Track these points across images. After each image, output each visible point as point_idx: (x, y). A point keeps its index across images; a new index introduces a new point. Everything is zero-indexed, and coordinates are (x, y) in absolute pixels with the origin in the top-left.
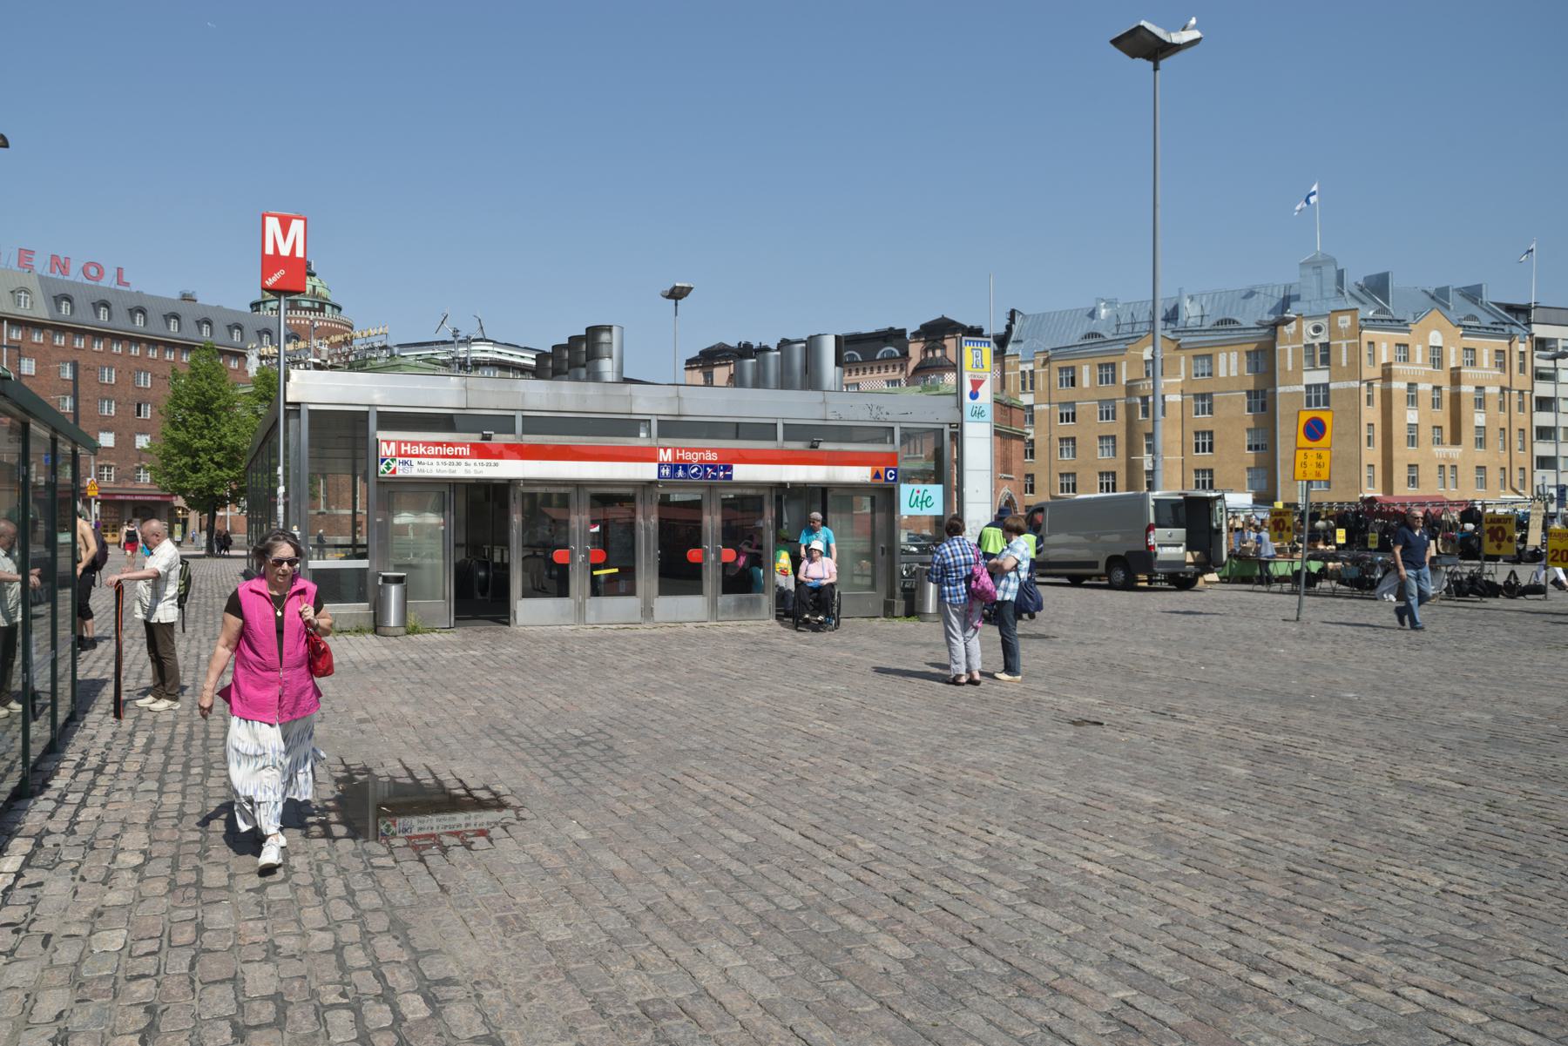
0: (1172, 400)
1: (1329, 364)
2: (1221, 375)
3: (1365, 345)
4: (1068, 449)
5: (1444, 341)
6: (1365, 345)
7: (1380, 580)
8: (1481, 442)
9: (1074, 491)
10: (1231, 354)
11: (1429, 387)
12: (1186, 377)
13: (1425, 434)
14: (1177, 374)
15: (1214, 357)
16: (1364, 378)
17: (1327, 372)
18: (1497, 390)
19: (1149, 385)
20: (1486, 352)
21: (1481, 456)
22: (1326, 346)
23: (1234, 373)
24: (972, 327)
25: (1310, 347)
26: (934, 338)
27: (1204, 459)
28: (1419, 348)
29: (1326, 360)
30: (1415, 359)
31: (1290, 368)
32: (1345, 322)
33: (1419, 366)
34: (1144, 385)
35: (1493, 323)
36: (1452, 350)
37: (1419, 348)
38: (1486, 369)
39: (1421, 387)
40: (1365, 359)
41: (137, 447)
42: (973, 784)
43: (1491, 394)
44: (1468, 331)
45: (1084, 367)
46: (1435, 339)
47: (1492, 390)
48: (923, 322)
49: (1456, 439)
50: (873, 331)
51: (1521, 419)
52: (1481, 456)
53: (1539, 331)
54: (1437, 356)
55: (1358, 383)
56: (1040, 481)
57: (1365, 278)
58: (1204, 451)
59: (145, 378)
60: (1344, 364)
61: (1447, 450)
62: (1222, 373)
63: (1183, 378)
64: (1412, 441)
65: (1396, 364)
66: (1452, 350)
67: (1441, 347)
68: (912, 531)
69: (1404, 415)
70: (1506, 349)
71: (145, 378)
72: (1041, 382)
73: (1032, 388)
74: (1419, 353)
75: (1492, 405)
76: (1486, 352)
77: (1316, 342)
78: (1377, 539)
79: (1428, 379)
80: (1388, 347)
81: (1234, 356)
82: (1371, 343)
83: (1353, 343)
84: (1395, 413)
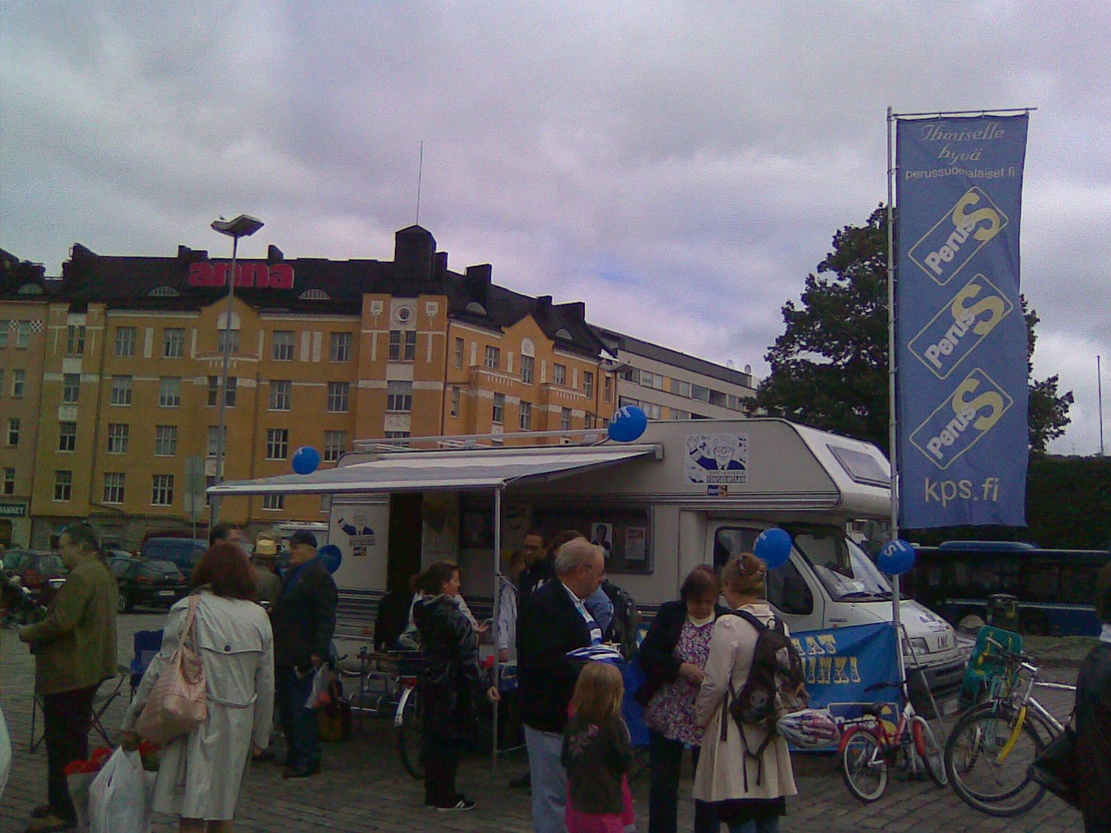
1: (414, 359)
3: (453, 342)
4: (118, 440)
6: (453, 342)
9: (121, 499)
10: (316, 333)
11: (517, 401)
16: (449, 380)
17: (411, 368)
19: (219, 362)
20: (575, 372)
22: (411, 336)
23: (317, 359)
25: (395, 334)
28: (510, 355)
29: (410, 353)
30: (506, 367)
31: (374, 358)
32: (431, 308)
33: (509, 375)
36: (544, 363)
37: (510, 355)
38: (574, 390)
39: (508, 399)
40: (453, 359)
42: (968, 738)
54: (528, 366)
55: (440, 386)
56: (79, 481)
57: (45, 269)
58: (277, 456)
59: (1011, 174)
62: (304, 357)
63: (261, 357)
65: (484, 369)
66: (544, 363)
67: (532, 359)
70: (594, 372)
71: (1011, 174)
72: (92, 345)
76: (575, 372)
77: (403, 329)
78: (373, 630)
80: (478, 349)
81: (318, 337)
82: (460, 340)
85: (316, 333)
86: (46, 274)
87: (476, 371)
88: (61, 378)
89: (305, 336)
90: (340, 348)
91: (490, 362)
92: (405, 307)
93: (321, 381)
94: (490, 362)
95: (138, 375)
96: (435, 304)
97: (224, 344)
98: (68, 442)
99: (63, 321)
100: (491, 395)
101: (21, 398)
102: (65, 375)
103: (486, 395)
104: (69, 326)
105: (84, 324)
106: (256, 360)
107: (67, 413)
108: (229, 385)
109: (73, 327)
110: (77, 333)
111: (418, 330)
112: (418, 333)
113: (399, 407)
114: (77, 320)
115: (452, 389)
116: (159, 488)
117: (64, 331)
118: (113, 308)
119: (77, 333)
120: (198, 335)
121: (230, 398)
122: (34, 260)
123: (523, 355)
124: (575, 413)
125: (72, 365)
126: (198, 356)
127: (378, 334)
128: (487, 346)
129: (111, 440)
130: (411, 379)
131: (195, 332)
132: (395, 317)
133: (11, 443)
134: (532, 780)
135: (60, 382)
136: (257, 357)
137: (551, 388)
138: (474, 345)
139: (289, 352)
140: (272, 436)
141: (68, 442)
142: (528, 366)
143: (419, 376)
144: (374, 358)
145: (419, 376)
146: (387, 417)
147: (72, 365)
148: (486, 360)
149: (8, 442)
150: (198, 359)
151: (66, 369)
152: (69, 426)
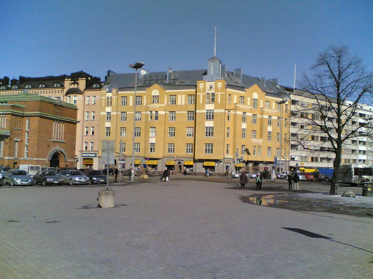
0: (161, 113)
2: (179, 104)
3: (227, 95)
5: (160, 94)
7: (16, 185)
8: (269, 138)
10: (183, 95)
11: (251, 114)
12: (167, 104)
13: (248, 133)
14: (163, 103)
15: (177, 96)
18: (276, 118)
21: (270, 143)
23: (183, 104)
24: (96, 77)
26: (75, 79)
27: (172, 139)
28: (249, 99)
30: (247, 103)
31: (201, 103)
32: (201, 85)
34: (151, 106)
35: (278, 93)
36: (262, 101)
41: (110, 123)
43: (274, 119)
44: (268, 94)
45: (131, 97)
46: (255, 96)
47: (275, 118)
48: (72, 73)
49: (261, 136)
50: (45, 76)
51: (285, 130)
52: (270, 143)
53: (293, 97)
54: (255, 102)
60: (219, 102)
61: (257, 140)
62: (179, 103)
63: (166, 104)
64: (244, 135)
68: (269, 180)
69: (241, 125)
72: (114, 102)
73: (111, 105)
74: (249, 101)
75: (275, 124)
77: (210, 92)
79: (250, 111)
81: (184, 96)
83: (223, 94)
84: (237, 124)
85: (183, 95)
86: (101, 81)
87: (236, 105)
88: (106, 114)
89: (179, 96)
90: (159, 99)
91: (242, 102)
92: (211, 85)
93: (186, 111)
94: (242, 102)
95: (128, 112)
96: (221, 83)
97: (156, 99)
98: (108, 134)
99: (105, 95)
100: (241, 113)
101: (94, 120)
102: (107, 112)
103: (240, 113)
104: (107, 97)
105: (111, 96)
106: (164, 105)
107: (108, 124)
108: (209, 111)
109: (108, 97)
110: (110, 99)
111: (113, 96)
112: (215, 93)
113: (210, 119)
114: (109, 95)
115: (227, 112)
116: (136, 147)
117: (106, 98)
118: (119, 91)
119: (110, 99)
120: (146, 98)
121: (157, 118)
122: (97, 76)
123: (254, 99)
124: (273, 118)
125: (108, 109)
126: (146, 104)
127: (202, 94)
128: (240, 96)
129: (121, 132)
130: (213, 109)
131: (145, 97)
132: (208, 87)
133: (292, 123)
134: (325, 236)
135: (105, 115)
136: (164, 104)
137: (264, 109)
138: (235, 96)
139: (174, 102)
140: (210, 129)
141: (108, 134)
142: (255, 102)
143: (216, 108)
144: (201, 103)
145: (216, 108)
146: (206, 121)
147: (108, 109)
148: (240, 101)
149: (91, 135)
150: (147, 106)
151: (107, 111)
152: (108, 128)
